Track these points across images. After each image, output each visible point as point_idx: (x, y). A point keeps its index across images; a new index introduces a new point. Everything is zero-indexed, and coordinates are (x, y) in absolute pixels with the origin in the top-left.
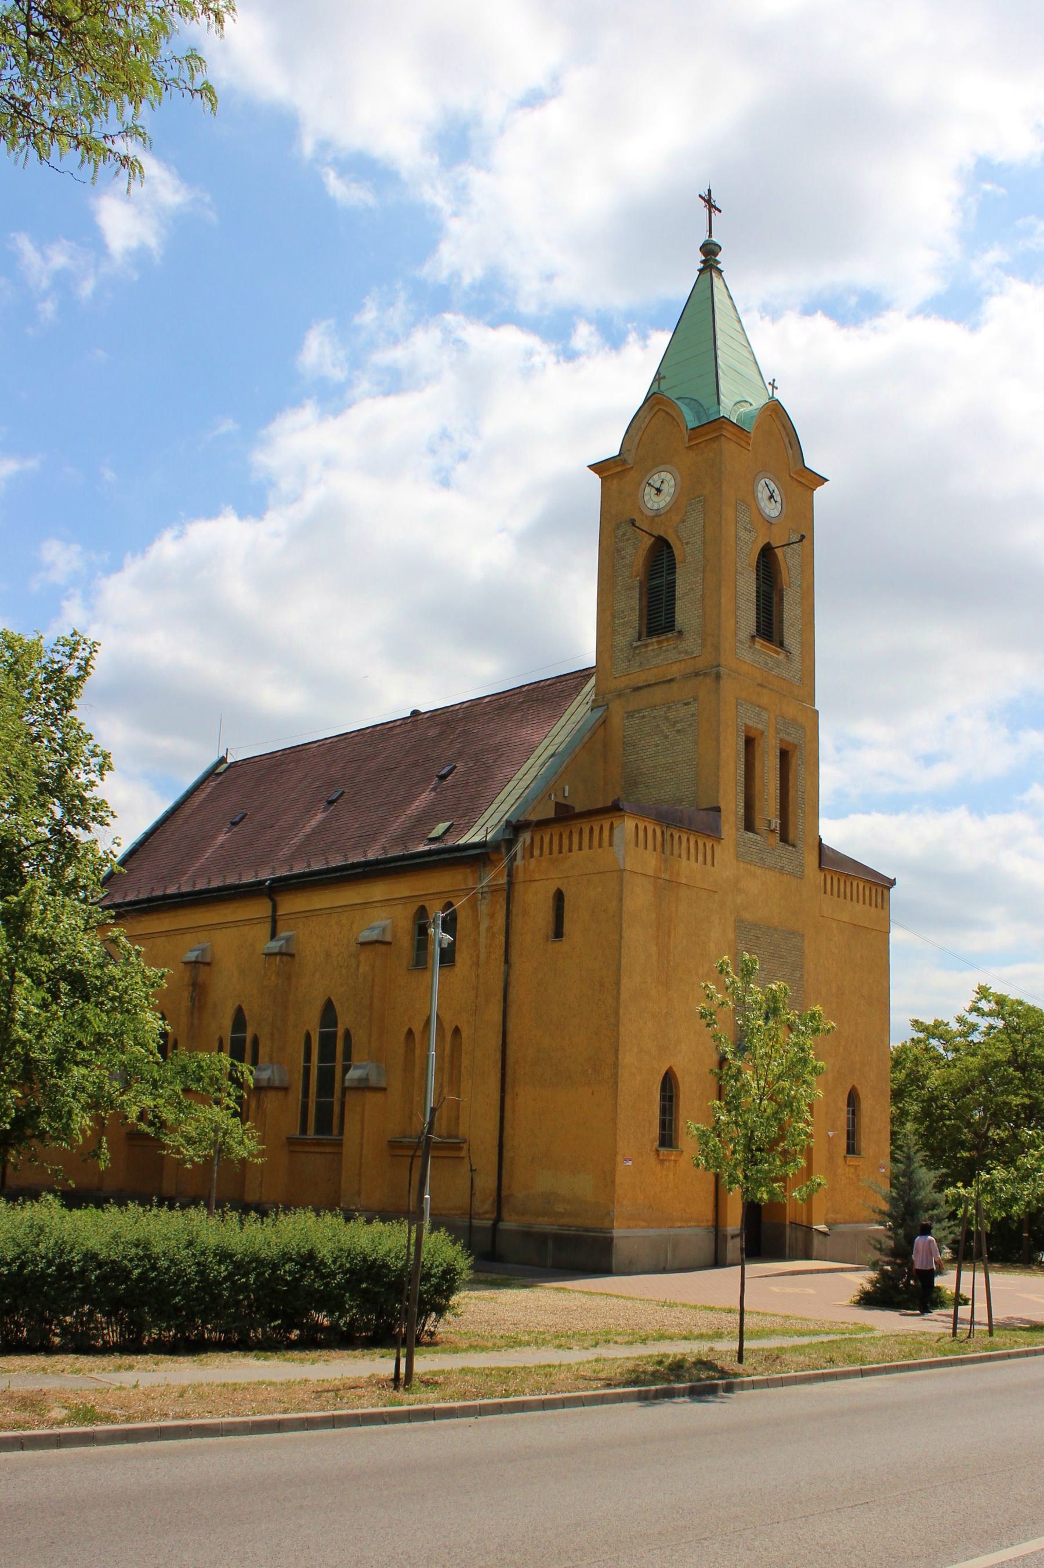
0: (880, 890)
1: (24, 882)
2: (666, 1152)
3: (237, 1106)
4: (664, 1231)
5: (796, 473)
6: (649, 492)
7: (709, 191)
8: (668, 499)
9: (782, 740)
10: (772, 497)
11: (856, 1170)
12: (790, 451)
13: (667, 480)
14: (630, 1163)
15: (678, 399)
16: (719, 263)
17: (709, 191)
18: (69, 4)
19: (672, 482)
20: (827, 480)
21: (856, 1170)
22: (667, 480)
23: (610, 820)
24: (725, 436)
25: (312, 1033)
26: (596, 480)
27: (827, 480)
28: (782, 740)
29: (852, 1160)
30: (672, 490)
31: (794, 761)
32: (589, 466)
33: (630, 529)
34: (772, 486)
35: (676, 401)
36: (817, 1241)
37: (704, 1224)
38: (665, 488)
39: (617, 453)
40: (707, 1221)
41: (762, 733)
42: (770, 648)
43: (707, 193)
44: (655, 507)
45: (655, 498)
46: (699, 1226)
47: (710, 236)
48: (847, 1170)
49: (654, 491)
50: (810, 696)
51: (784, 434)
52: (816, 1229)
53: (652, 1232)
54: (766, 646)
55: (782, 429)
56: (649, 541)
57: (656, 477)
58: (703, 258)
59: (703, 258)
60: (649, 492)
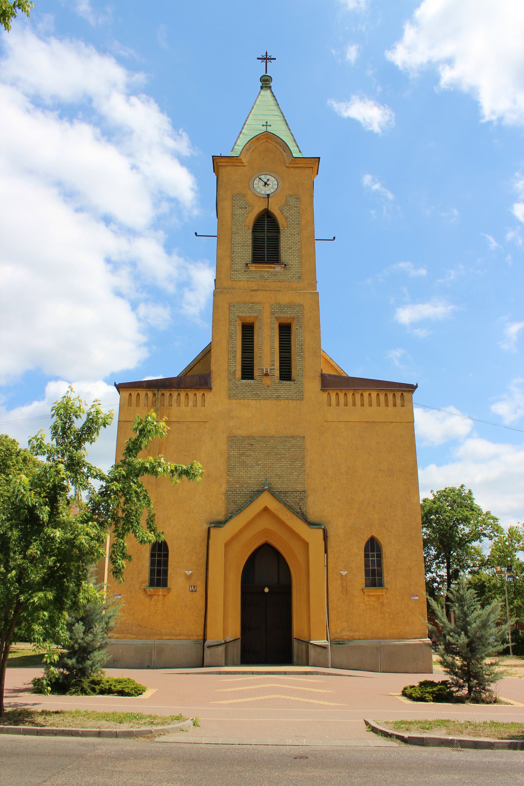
0: (398, 395)
1: (82, 543)
2: (152, 590)
3: (61, 670)
4: (150, 642)
5: (290, 163)
9: (277, 318)
12: (285, 154)
23: (130, 392)
24: (221, 166)
25: (422, 680)
28: (277, 318)
36: (312, 652)
37: (195, 637)
40: (198, 636)
41: (257, 317)
42: (271, 267)
46: (189, 639)
48: (367, 599)
50: (313, 284)
51: (278, 147)
52: (312, 644)
53: (138, 642)
54: (257, 266)
55: (276, 145)
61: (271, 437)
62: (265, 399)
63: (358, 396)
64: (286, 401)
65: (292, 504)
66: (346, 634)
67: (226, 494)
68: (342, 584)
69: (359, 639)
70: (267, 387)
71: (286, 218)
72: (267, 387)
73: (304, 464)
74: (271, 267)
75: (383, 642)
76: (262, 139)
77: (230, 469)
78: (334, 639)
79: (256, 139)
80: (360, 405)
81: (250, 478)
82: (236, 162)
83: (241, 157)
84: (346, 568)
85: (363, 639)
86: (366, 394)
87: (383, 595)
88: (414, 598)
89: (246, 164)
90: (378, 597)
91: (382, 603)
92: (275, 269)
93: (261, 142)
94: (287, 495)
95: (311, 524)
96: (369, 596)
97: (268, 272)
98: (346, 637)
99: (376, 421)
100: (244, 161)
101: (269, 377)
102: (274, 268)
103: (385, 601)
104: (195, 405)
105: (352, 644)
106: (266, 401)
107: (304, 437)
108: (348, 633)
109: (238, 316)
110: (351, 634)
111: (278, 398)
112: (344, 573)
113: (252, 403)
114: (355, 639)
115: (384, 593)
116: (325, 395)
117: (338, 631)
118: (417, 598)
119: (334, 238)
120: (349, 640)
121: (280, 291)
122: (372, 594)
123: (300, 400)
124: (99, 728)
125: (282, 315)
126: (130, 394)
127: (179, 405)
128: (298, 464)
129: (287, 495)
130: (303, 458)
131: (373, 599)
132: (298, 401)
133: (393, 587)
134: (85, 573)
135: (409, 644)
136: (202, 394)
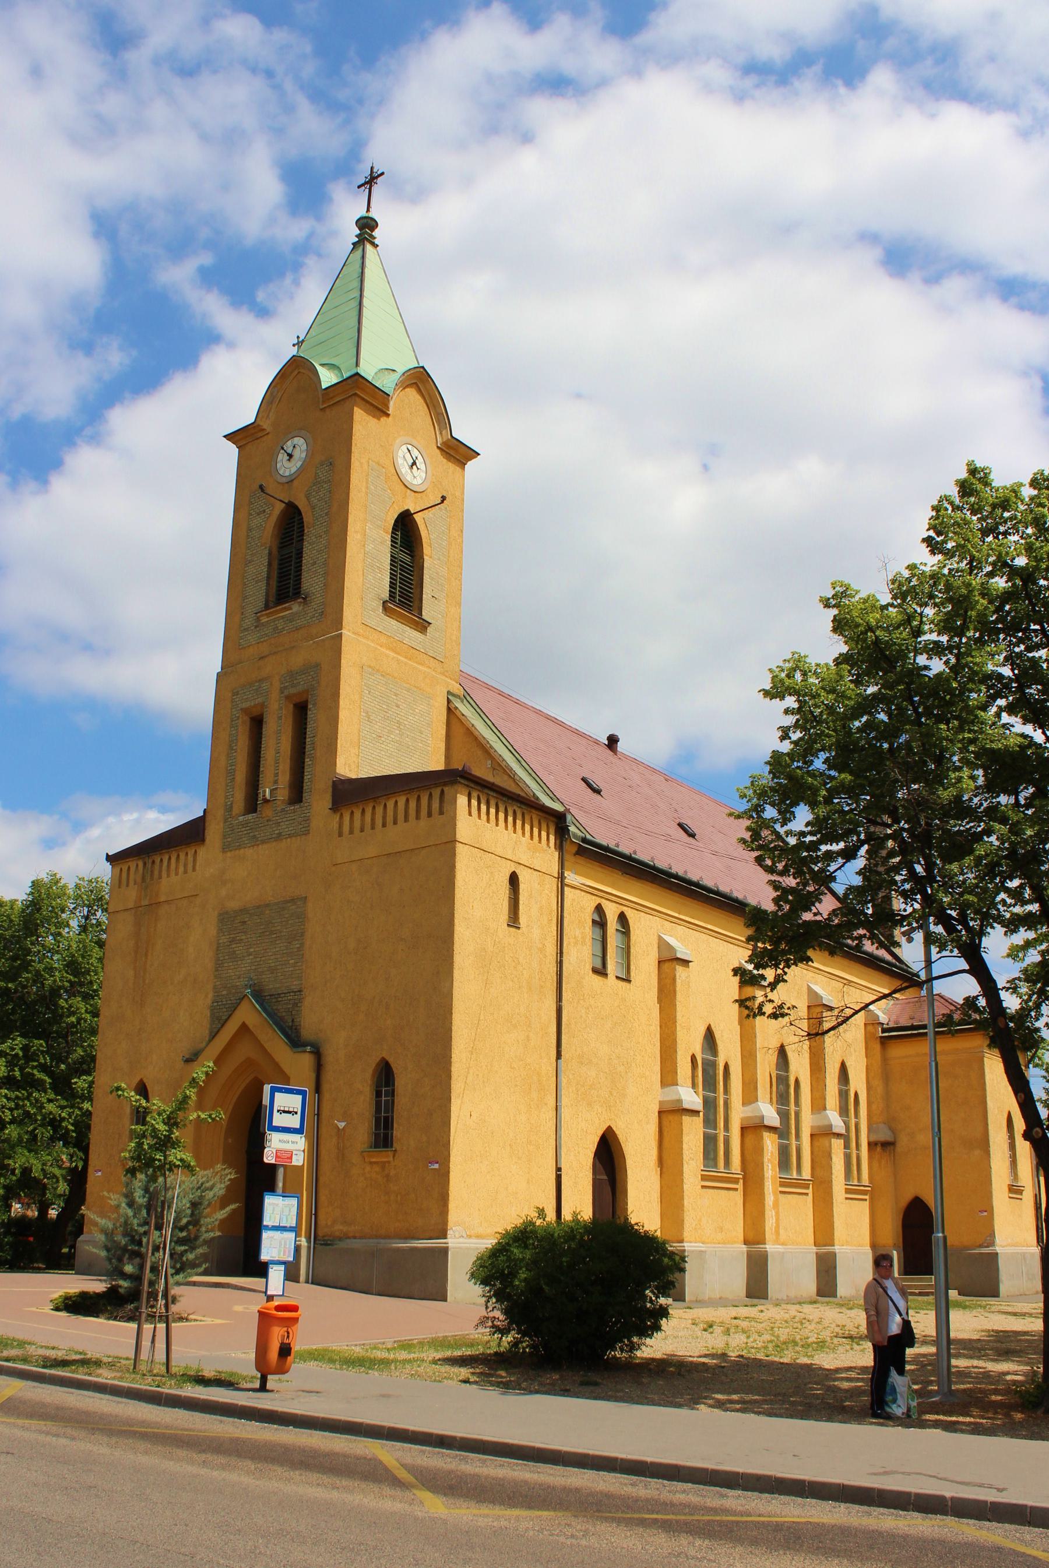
5: (324, 402)
6: (282, 457)
7: (382, 174)
8: (299, 464)
10: (414, 463)
11: (383, 1168)
13: (299, 446)
14: (100, 1174)
15: (322, 365)
16: (375, 238)
17: (382, 174)
18: (1047, 563)
19: (304, 447)
20: (479, 454)
21: (383, 1168)
22: (299, 446)
26: (232, 451)
27: (479, 454)
28: (287, 698)
29: (383, 1156)
30: (304, 455)
31: (316, 716)
32: (225, 436)
33: (259, 493)
34: (415, 453)
35: (319, 369)
38: (297, 454)
39: (253, 421)
42: (285, 608)
43: (379, 173)
44: (287, 474)
45: (287, 464)
47: (368, 210)
48: (368, 1169)
49: (286, 457)
54: (274, 612)
56: (279, 507)
57: (289, 443)
58: (358, 232)
59: (358, 232)
60: (282, 457)
61: (267, 905)
62: (263, 842)
63: (379, 810)
64: (289, 840)
65: (284, 1014)
66: (339, 1228)
67: (212, 1009)
68: (338, 1143)
69: (355, 1237)
70: (268, 821)
71: (313, 508)
72: (268, 821)
73: (302, 945)
74: (286, 609)
75: (384, 1243)
76: (292, 373)
77: (219, 965)
78: (324, 1236)
79: (280, 378)
80: (381, 825)
81: (239, 978)
82: (256, 433)
83: (259, 422)
84: (345, 1117)
85: (361, 1238)
86: (402, 801)
87: (389, 1162)
88: (432, 1167)
89: (268, 430)
90: (383, 1165)
91: (388, 1176)
92: (291, 609)
93: (291, 378)
94: (280, 999)
95: (296, 1041)
96: (371, 1163)
97: (283, 617)
98: (337, 1234)
99: (400, 850)
100: (265, 427)
101: (270, 803)
102: (290, 608)
103: (393, 1173)
104: (185, 872)
105: (342, 1245)
106: (265, 846)
107: (306, 897)
108: (341, 1227)
109: (241, 709)
110: (345, 1229)
111: (279, 837)
112: (341, 1125)
113: (249, 852)
114: (349, 1238)
115: (391, 1159)
116: (337, 817)
117: (329, 1224)
118: (436, 1166)
119: (444, 498)
120: (340, 1239)
121: (293, 647)
122: (374, 1160)
123: (306, 834)
124: (81, 1353)
125: (293, 691)
126: (121, 869)
127: (168, 876)
128: (296, 945)
129: (280, 999)
130: (302, 934)
131: (377, 1169)
132: (304, 837)
133: (405, 1148)
134: (913, 1400)
135: (416, 1248)
136: (193, 851)
